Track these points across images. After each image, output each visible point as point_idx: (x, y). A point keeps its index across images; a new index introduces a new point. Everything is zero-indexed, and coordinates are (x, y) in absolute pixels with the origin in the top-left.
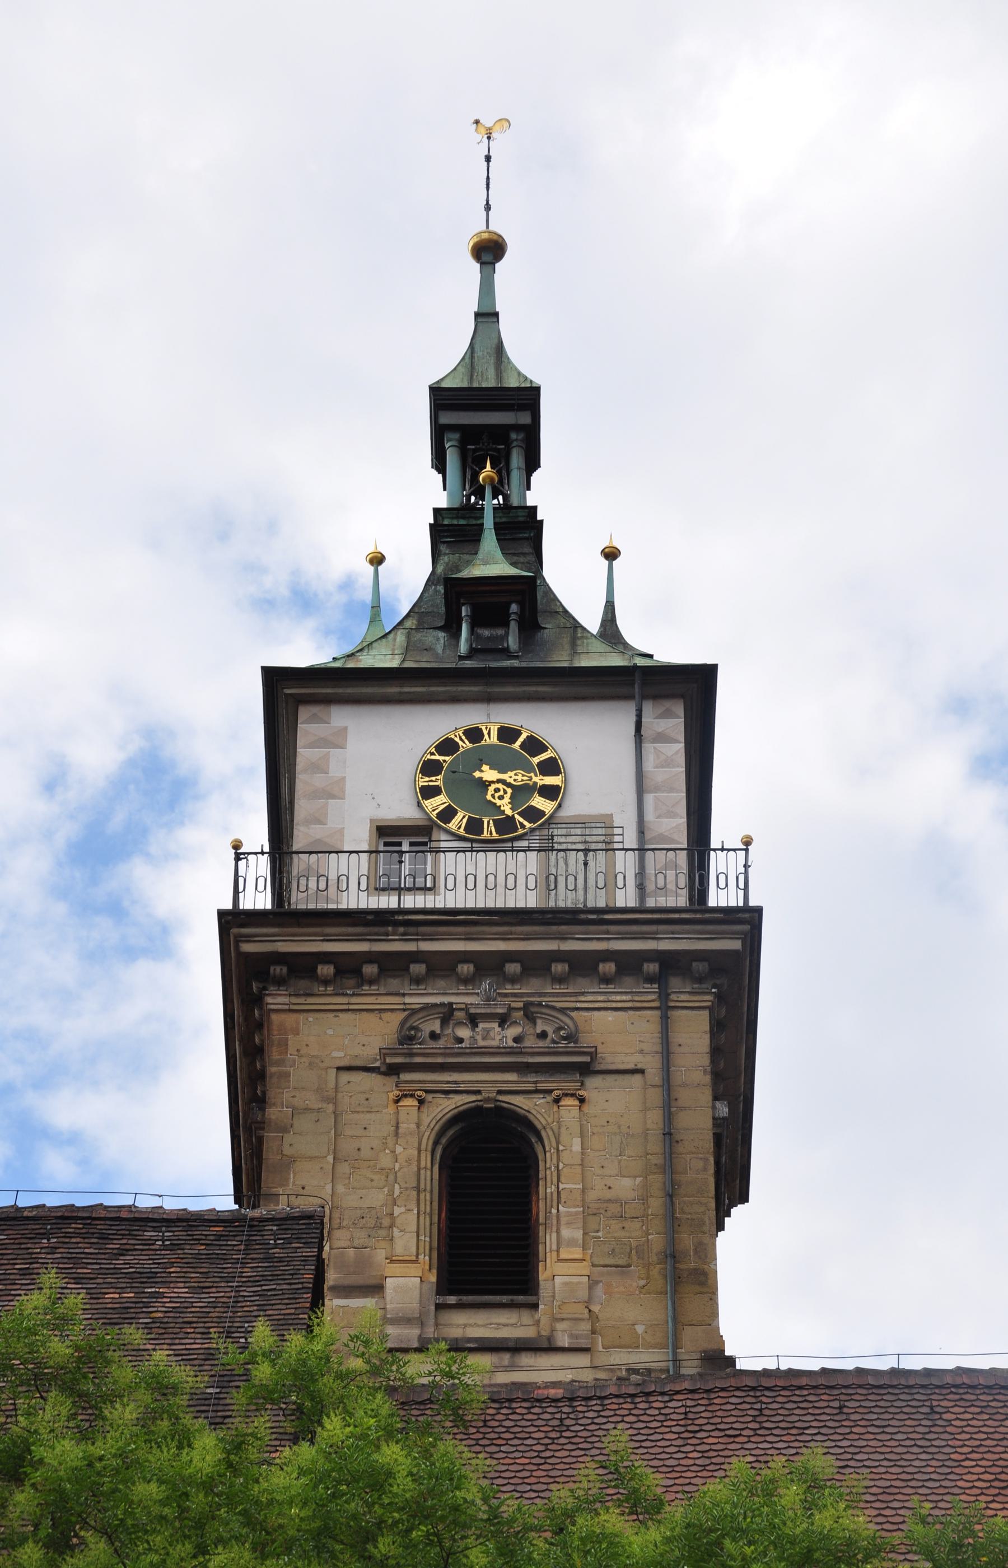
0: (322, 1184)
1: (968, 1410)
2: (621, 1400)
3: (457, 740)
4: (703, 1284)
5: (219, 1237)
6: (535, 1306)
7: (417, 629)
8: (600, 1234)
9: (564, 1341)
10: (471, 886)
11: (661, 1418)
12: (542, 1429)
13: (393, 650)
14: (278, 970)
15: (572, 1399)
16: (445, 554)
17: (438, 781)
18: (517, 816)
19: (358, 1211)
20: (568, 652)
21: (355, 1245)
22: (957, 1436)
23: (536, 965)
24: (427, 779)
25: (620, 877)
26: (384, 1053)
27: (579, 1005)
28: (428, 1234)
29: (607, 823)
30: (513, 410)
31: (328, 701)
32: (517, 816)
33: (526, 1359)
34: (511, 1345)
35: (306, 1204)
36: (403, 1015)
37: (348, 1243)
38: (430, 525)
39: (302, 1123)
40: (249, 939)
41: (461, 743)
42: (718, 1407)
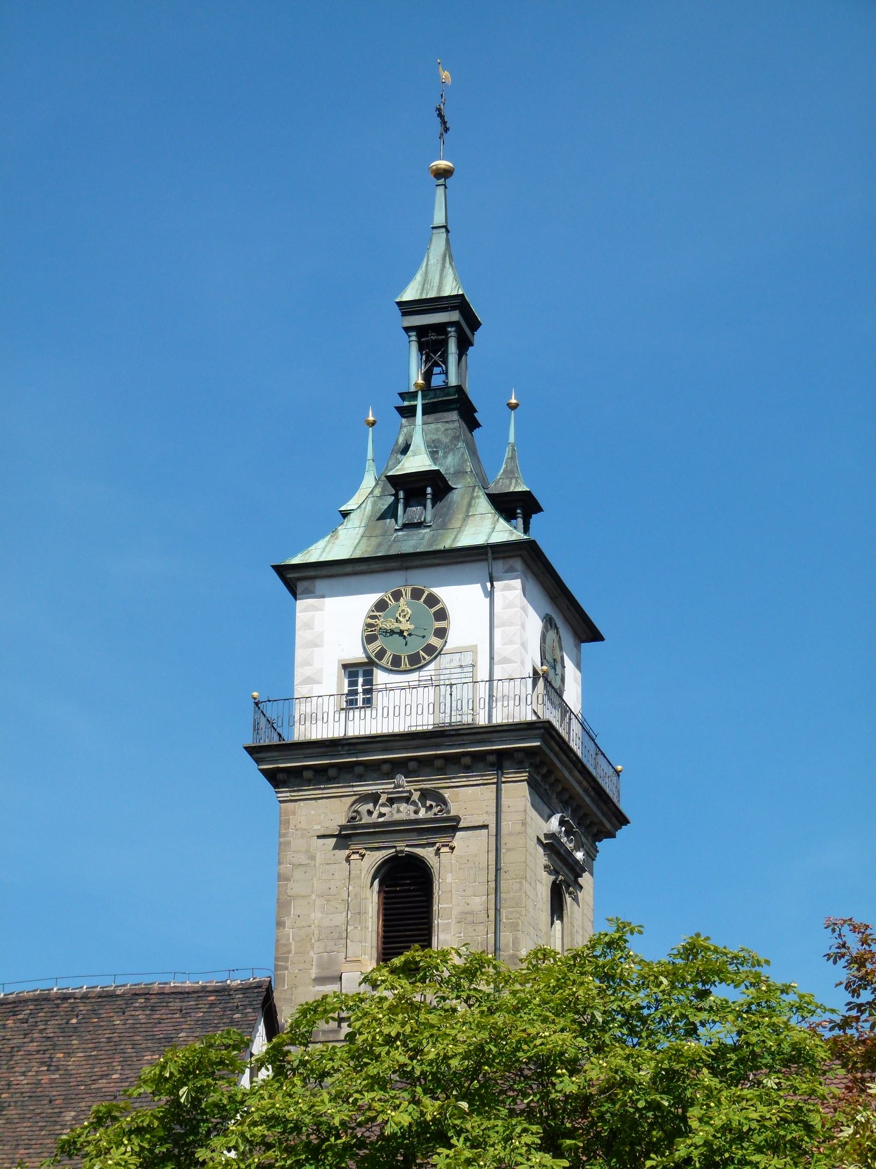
5: (212, 1005)
26: (343, 828)
31: (314, 578)
37: (323, 950)
39: (298, 874)
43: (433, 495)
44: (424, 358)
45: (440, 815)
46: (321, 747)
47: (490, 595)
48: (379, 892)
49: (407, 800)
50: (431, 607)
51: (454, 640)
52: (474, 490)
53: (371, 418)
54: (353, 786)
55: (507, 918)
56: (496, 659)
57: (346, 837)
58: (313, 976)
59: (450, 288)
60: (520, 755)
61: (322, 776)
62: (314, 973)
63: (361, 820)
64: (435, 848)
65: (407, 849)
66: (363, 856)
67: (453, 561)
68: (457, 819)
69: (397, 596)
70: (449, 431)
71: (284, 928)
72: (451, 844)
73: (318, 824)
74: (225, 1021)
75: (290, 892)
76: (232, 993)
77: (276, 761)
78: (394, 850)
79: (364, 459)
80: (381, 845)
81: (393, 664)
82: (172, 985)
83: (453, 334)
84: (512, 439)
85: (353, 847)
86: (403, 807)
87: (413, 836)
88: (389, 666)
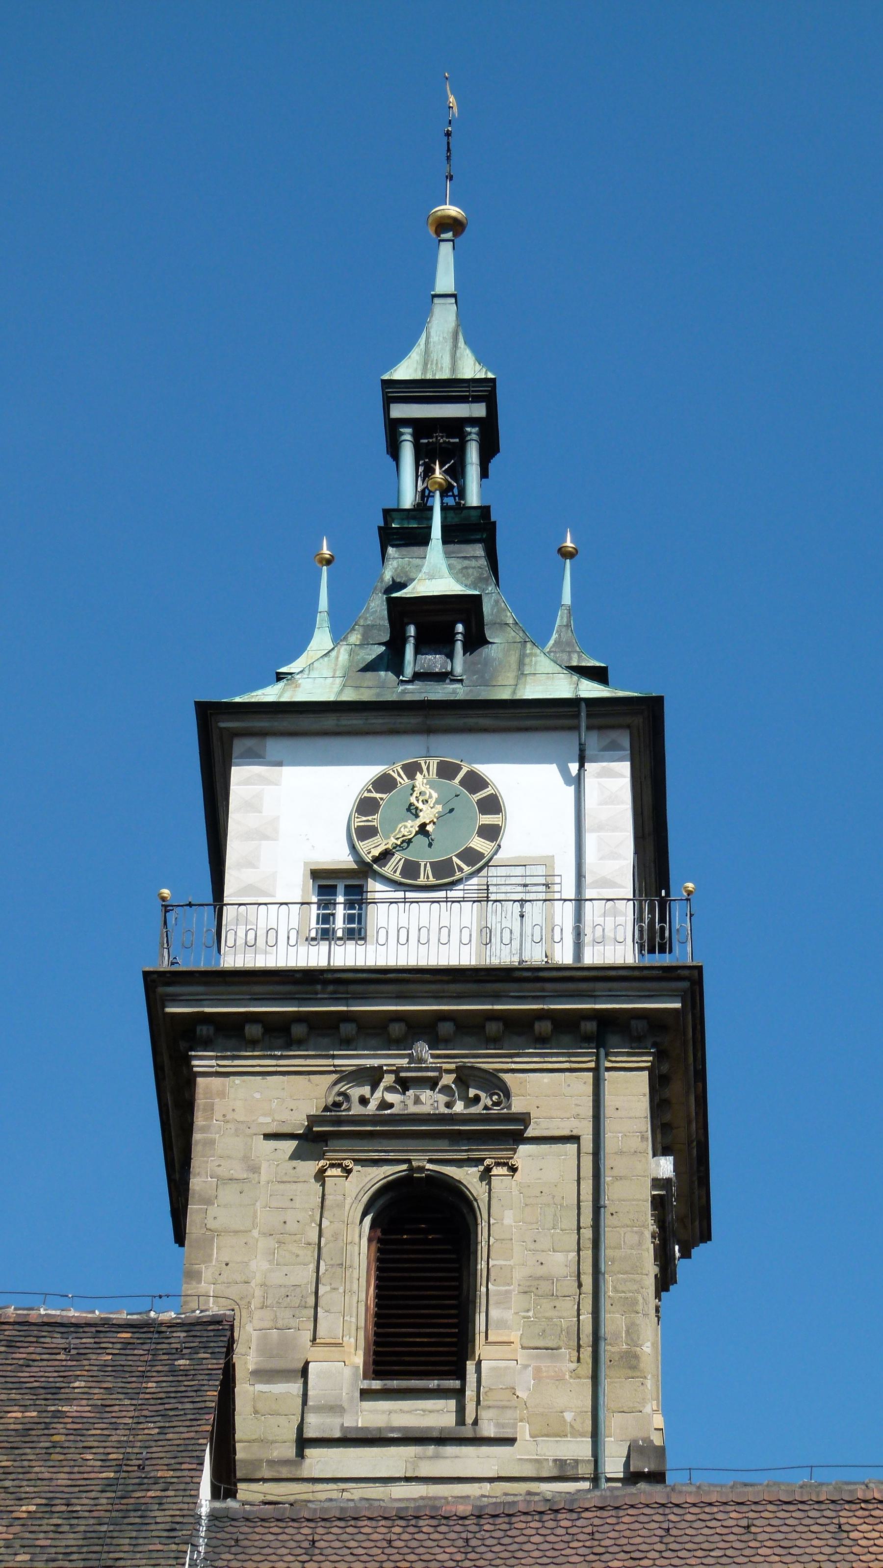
0: (246, 1260)
1: (876, 1527)
2: (529, 1518)
3: (395, 776)
4: (634, 1368)
5: (126, 1344)
7: (361, 645)
8: (531, 1314)
10: (403, 940)
11: (567, 1538)
12: (447, 1550)
13: (335, 671)
14: (204, 1030)
15: (479, 1517)
16: (394, 558)
18: (455, 859)
19: (282, 1289)
20: (514, 674)
21: (278, 1326)
22: (862, 1558)
24: (364, 819)
25: (557, 930)
26: (313, 1120)
27: (513, 1066)
28: (354, 1314)
30: (468, 402)
31: (263, 734)
32: (455, 859)
33: (450, 1450)
34: (435, 1434)
35: (214, 1309)
36: (335, 1077)
38: (380, 528)
39: (227, 1194)
40: (176, 999)
41: (399, 779)
42: (626, 1526)
43: (466, 635)
44: (421, 469)
45: (496, 1110)
46: (283, 983)
48: (370, 1240)
49: (432, 1084)
50: (473, 791)
51: (512, 845)
52: (525, 647)
53: (326, 552)
54: (333, 1057)
55: (615, 1290)
57: (315, 1140)
58: (251, 1367)
59: (470, 369)
60: (639, 1026)
61: (279, 1035)
63: (349, 1109)
64: (481, 1168)
65: (429, 1166)
66: (349, 1172)
67: (515, 723)
68: (524, 1119)
69: (411, 770)
70: (470, 571)
71: (200, 1282)
72: (511, 1162)
73: (265, 1115)
74: (160, 1368)
75: (211, 1224)
76: (163, 1329)
77: (198, 1002)
78: (404, 1167)
79: (315, 611)
80: (383, 1155)
81: (404, 874)
82: (42, 1312)
83: (474, 437)
84: (567, 598)
85: (329, 1155)
86: (426, 1095)
87: (443, 1144)
88: (397, 877)
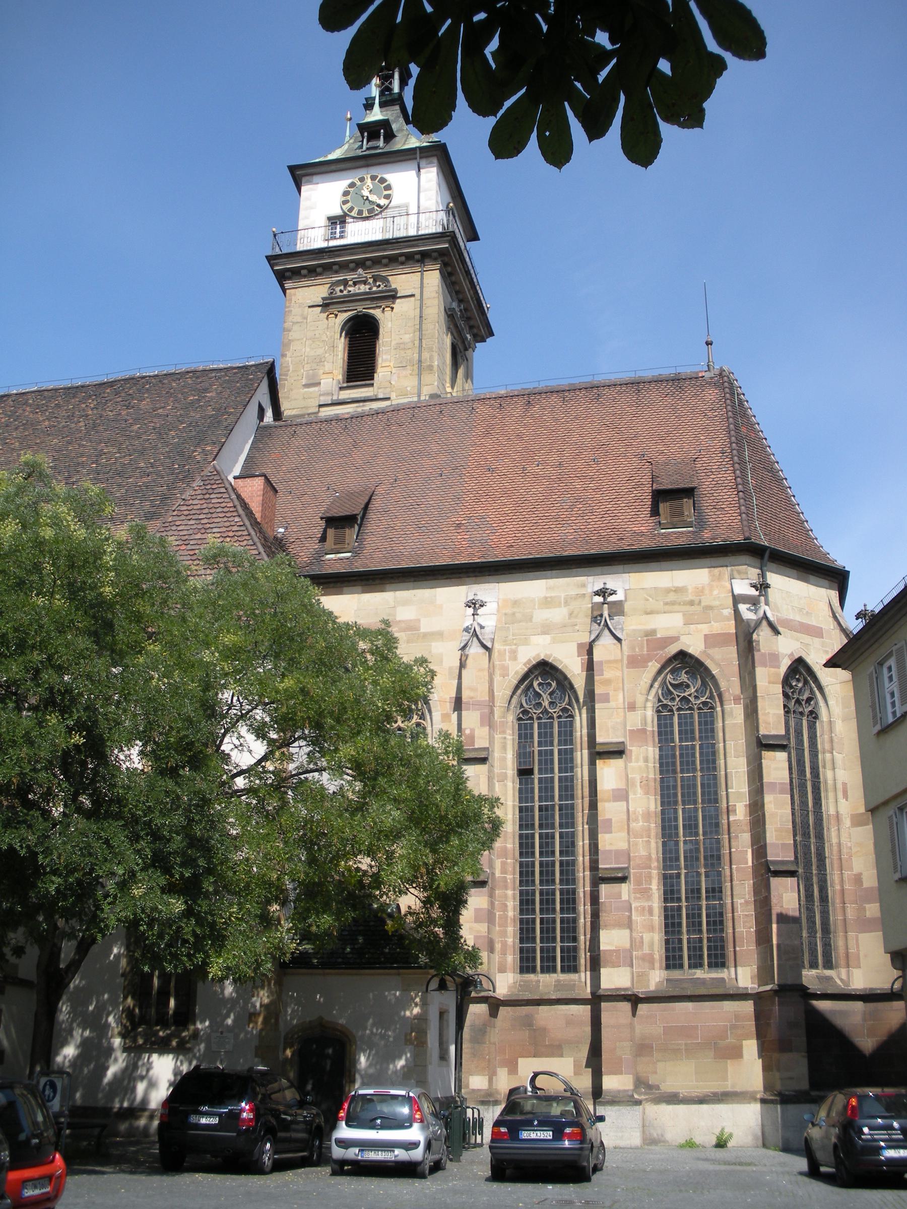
4: (497, 1160)
5: (235, 373)
6: (372, 385)
9: (381, 396)
14: (288, 274)
17: (349, 198)
23: (376, 262)
29: (407, 206)
31: (312, 174)
39: (295, 328)
47: (419, 175)
56: (421, 189)
57: (326, 305)
61: (312, 272)
62: (304, 382)
66: (336, 315)
